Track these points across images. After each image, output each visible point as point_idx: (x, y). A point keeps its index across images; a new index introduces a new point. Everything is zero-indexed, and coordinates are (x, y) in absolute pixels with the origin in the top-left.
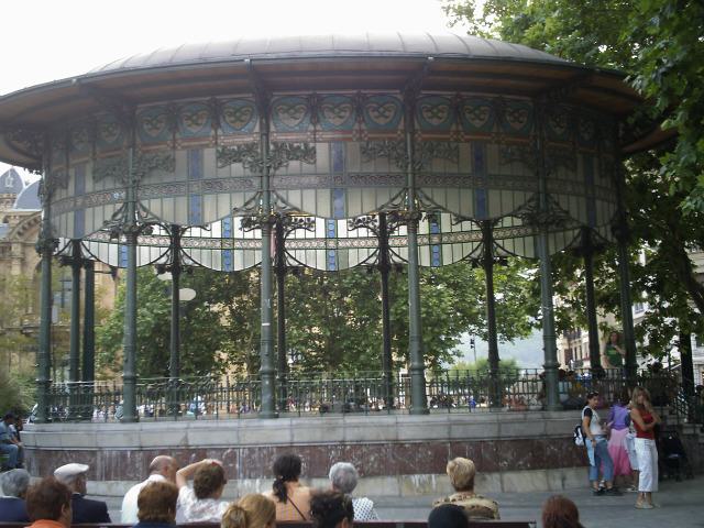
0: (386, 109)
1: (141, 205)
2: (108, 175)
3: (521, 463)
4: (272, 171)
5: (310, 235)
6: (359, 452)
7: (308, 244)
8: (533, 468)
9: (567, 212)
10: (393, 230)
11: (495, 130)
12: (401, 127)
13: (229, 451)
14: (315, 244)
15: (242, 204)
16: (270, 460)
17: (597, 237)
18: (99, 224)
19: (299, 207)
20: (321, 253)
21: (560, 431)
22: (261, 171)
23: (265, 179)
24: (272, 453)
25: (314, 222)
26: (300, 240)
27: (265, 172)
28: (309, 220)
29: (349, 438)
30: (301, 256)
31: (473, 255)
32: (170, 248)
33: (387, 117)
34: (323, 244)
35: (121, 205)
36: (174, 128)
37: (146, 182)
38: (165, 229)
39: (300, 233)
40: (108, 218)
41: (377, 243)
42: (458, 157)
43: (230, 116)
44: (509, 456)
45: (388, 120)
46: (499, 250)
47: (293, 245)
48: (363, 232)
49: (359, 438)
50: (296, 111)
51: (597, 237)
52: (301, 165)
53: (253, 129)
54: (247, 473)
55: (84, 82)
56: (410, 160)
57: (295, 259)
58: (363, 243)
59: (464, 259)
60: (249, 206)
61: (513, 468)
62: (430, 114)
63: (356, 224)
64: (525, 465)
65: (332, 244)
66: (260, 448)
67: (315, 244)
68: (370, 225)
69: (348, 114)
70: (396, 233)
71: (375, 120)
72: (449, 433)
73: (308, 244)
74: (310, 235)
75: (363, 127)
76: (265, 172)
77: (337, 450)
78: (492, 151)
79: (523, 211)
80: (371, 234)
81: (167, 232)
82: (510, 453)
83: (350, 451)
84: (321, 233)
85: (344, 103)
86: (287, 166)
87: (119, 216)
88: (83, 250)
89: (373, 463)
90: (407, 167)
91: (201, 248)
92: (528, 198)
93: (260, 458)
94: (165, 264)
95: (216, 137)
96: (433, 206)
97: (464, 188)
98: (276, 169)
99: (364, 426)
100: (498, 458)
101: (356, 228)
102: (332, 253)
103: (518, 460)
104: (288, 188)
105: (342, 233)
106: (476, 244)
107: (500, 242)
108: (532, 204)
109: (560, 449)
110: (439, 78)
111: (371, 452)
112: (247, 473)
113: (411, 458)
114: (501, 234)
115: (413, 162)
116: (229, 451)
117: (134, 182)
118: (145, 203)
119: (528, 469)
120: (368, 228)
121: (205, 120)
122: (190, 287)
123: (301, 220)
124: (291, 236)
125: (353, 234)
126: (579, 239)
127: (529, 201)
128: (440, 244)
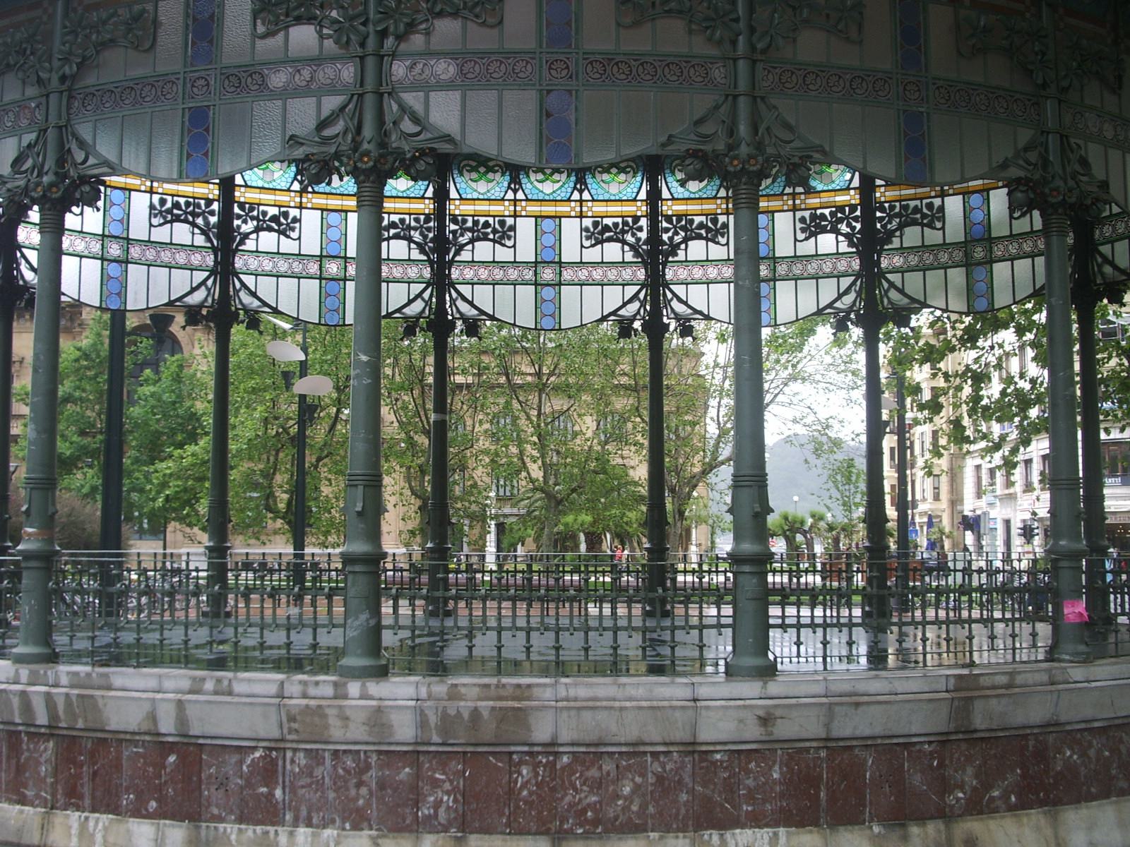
1: (75, 135)
2: (9, 67)
3: (996, 794)
4: (389, 42)
5: (504, 254)
6: (593, 773)
8: (1023, 805)
9: (1104, 185)
10: (674, 249)
13: (257, 754)
14: (513, 274)
15: (312, 124)
16: (360, 784)
17: (1108, 269)
19: (458, 138)
20: (526, 293)
21: (1088, 713)
22: (362, 45)
23: (370, 62)
24: (368, 767)
25: (513, 228)
27: (371, 43)
28: (930, 206)
29: (565, 736)
32: (213, 272)
34: (529, 275)
35: (33, 136)
37: (91, 80)
38: (203, 232)
39: (483, 250)
41: (641, 274)
44: (969, 777)
47: (469, 274)
48: (613, 251)
49: (593, 737)
51: (1108, 269)
52: (464, 29)
54: (304, 812)
56: (742, 25)
58: (612, 274)
60: (327, 132)
61: (978, 807)
65: (548, 274)
66: (336, 753)
67: (513, 274)
68: (629, 238)
72: (827, 726)
74: (504, 254)
76: (371, 43)
77: (536, 765)
79: (1015, 172)
80: (629, 256)
81: (209, 239)
83: (569, 768)
84: (526, 251)
86: (428, 33)
87: (29, 164)
89: (629, 799)
90: (734, 43)
92: (1022, 143)
93: (336, 778)
94: (201, 305)
98: (400, 38)
99: (592, 705)
100: (944, 786)
101: (601, 242)
102: (548, 293)
103: (988, 787)
104: (426, 87)
105: (570, 251)
108: (1033, 156)
109: (1083, 754)
111: (621, 773)
112: (304, 812)
113: (730, 788)
115: (752, 30)
116: (257, 754)
117: (63, 79)
118: (85, 131)
119: (1011, 808)
120: (624, 242)
123: (486, 225)
124: (465, 256)
125: (593, 254)
127: (1026, 149)
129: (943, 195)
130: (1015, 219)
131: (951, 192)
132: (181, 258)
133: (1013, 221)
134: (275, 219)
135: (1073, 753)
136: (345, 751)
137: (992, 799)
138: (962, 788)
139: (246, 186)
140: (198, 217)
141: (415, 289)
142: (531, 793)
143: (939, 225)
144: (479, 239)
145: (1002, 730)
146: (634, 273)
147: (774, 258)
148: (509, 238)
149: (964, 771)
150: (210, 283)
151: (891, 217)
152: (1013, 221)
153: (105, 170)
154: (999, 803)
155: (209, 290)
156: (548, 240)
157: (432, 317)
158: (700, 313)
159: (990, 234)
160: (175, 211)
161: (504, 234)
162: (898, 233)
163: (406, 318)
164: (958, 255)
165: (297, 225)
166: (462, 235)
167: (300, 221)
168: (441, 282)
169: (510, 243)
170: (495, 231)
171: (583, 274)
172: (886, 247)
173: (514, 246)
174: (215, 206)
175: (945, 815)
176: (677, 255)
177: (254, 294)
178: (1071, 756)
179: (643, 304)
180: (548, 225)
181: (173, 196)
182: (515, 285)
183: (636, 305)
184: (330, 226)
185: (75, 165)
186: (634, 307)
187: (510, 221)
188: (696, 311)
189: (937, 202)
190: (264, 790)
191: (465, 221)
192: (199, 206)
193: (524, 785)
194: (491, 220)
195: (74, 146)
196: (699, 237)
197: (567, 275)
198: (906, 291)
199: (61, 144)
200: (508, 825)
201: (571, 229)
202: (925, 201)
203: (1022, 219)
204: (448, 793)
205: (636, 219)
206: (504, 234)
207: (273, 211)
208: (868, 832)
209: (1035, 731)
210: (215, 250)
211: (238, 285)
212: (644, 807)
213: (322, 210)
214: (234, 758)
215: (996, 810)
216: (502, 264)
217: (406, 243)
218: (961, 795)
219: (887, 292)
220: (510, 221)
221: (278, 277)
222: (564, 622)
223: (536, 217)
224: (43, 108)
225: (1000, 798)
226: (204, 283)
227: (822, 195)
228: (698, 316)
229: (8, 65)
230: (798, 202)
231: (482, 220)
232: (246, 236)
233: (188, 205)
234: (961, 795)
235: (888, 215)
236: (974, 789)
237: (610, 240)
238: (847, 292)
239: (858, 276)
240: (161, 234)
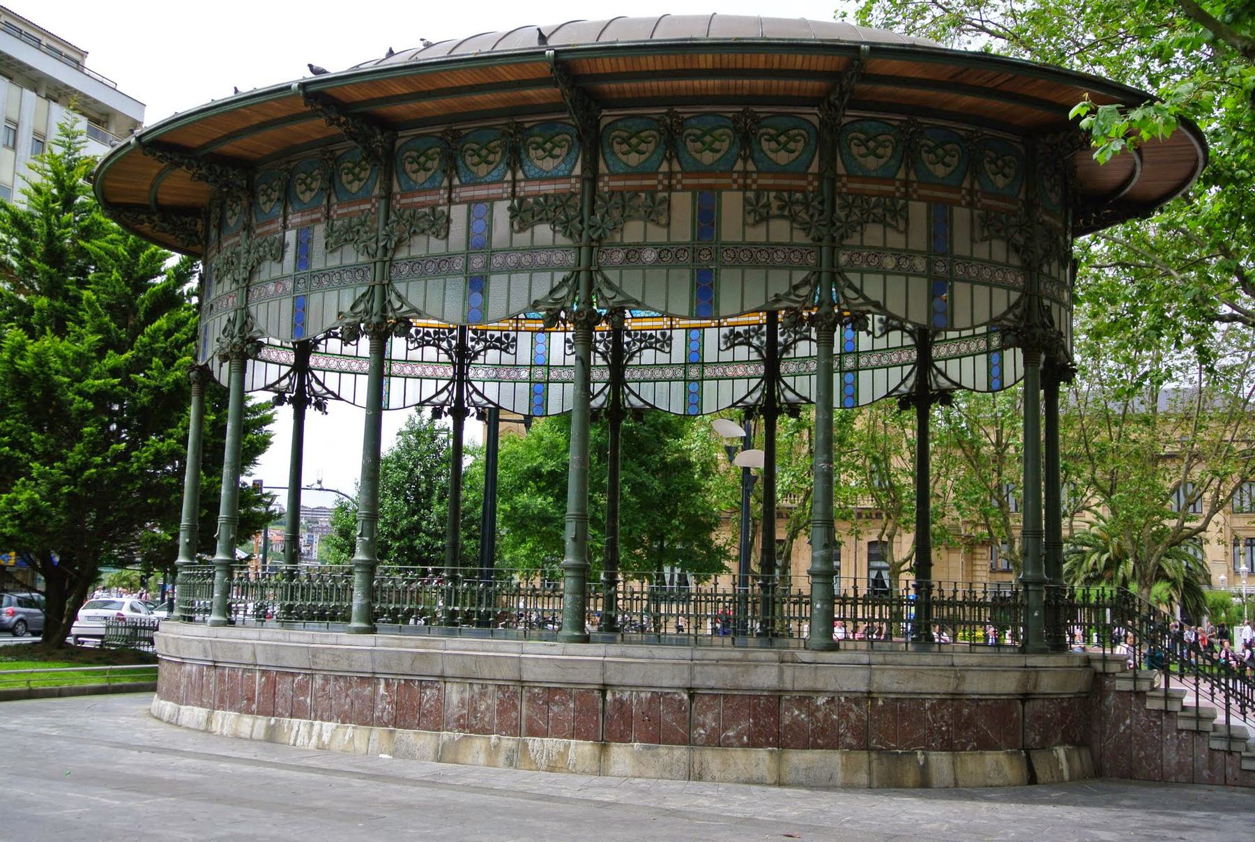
0: (715, 139)
3: (731, 734)
5: (662, 358)
7: (658, 374)
8: (753, 744)
10: (787, 348)
11: (739, 166)
12: (814, 168)
14: (669, 373)
16: (347, 696)
18: (331, 320)
20: (678, 387)
25: (515, 340)
30: (647, 391)
31: (748, 400)
33: (718, 151)
34: (680, 374)
36: (451, 164)
38: (446, 352)
39: (648, 356)
40: (346, 308)
41: (762, 370)
42: (907, 221)
43: (928, 152)
44: (709, 720)
47: (637, 375)
48: (742, 352)
53: (571, 171)
55: (311, 89)
57: (638, 397)
58: (740, 371)
59: (734, 405)
61: (715, 741)
62: (625, 147)
63: (733, 339)
64: (739, 737)
65: (694, 372)
67: (669, 373)
71: (772, 156)
73: (658, 374)
74: (662, 358)
75: (751, 167)
78: (731, 204)
81: (450, 357)
82: (710, 716)
84: (678, 355)
85: (721, 127)
87: (361, 307)
91: (670, 380)
95: (514, 182)
96: (619, 298)
97: (675, 267)
102: (693, 387)
103: (725, 729)
105: (710, 355)
106: (754, 382)
110: (760, 83)
120: (750, 345)
121: (498, 156)
124: (635, 361)
125: (727, 356)
126: (910, 382)
128: (856, 370)
134: (499, 340)
135: (800, 710)
136: (340, 676)
137: (728, 738)
138: (703, 726)
139: (633, 318)
140: (443, 341)
141: (442, 384)
142: (431, 706)
143: (667, 350)
145: (737, 690)
146: (445, 371)
147: (858, 352)
149: (705, 715)
150: (450, 388)
153: (415, 314)
154: (733, 740)
155: (449, 392)
156: (540, 349)
157: (453, 405)
158: (804, 398)
160: (426, 338)
161: (667, 341)
162: (638, 354)
163: (434, 405)
168: (617, 381)
169: (512, 351)
170: (657, 341)
171: (719, 372)
172: (936, 339)
173: (515, 353)
174: (765, 328)
175: (687, 741)
176: (789, 353)
177: (482, 395)
178: (799, 715)
179: (451, 393)
180: (694, 334)
181: (424, 327)
182: (421, 379)
183: (446, 394)
184: (691, 340)
185: (393, 310)
187: (513, 334)
188: (329, 392)
190: (302, 698)
191: (636, 335)
192: (444, 333)
193: (427, 701)
194: (654, 332)
195: (393, 297)
196: (495, 347)
197: (708, 372)
198: (797, 391)
199: (383, 298)
200: (418, 725)
201: (711, 335)
204: (389, 703)
205: (760, 326)
207: (497, 334)
208: (630, 748)
209: (766, 693)
210: (453, 364)
211: (471, 389)
212: (492, 718)
213: (532, 332)
214: (291, 679)
215: (731, 745)
216: (661, 366)
218: (702, 732)
220: (513, 334)
221: (718, 380)
223: (686, 329)
224: (372, 270)
225: (735, 737)
226: (446, 388)
228: (329, 396)
229: (346, 240)
232: (478, 353)
233: (435, 333)
234: (702, 732)
236: (713, 729)
237: (741, 344)
239: (626, 365)
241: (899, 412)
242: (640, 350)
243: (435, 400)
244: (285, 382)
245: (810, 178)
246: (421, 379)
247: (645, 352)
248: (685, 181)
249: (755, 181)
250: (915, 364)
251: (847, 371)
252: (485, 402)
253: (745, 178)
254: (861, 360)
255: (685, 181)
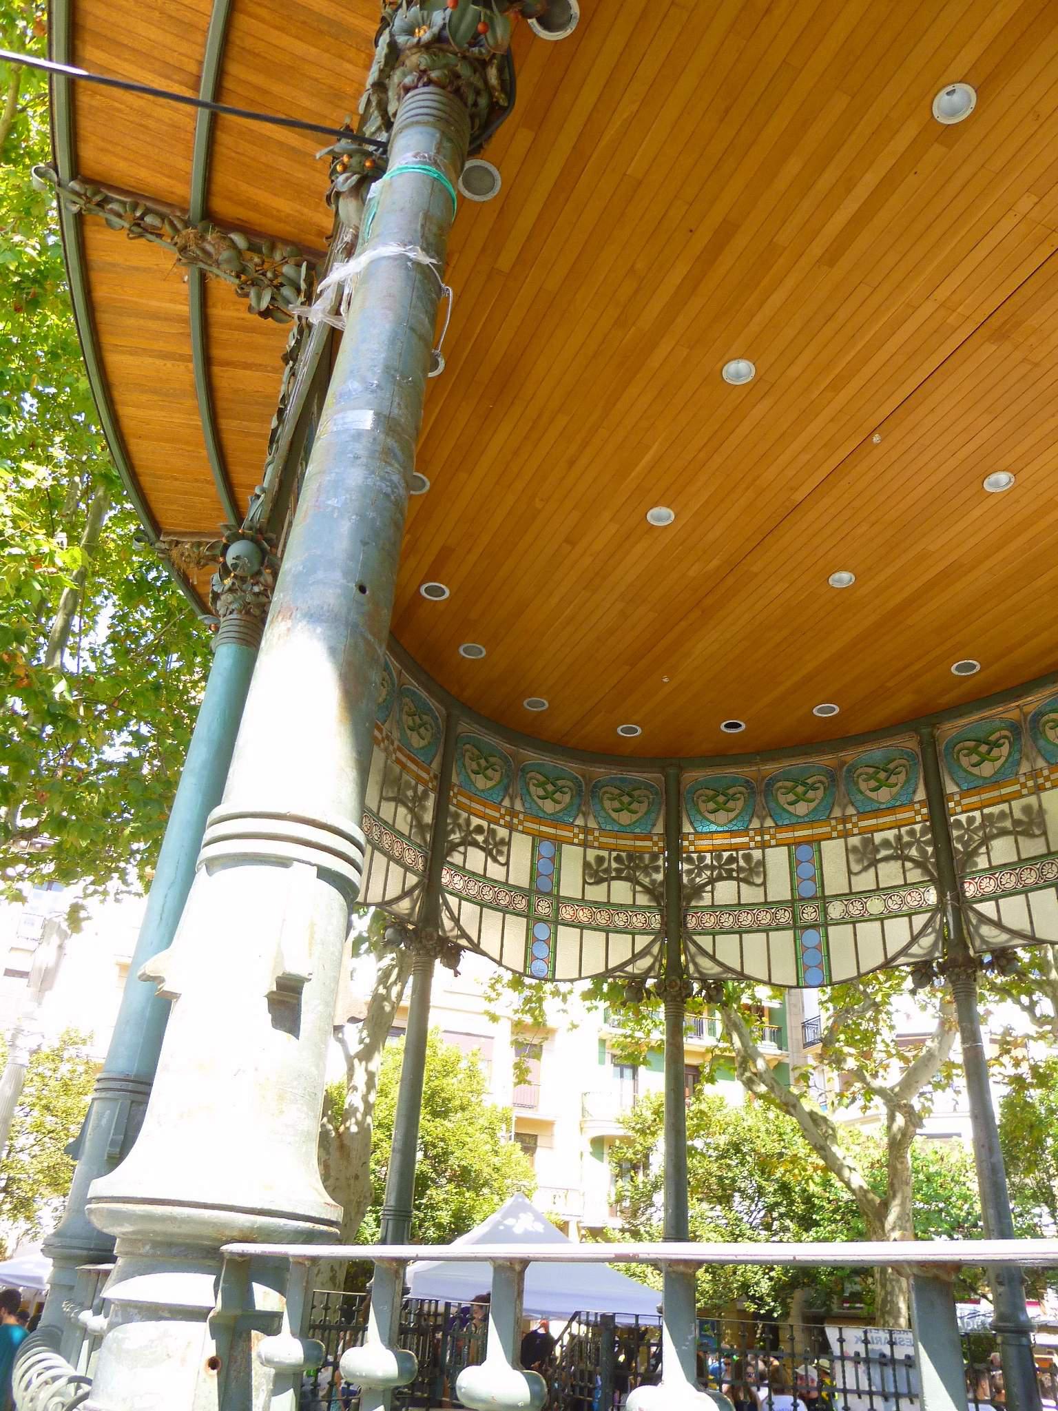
10: (698, 891)
25: (762, 863)
26: (621, 907)
28: (748, 858)
38: (918, 864)
39: (725, 892)
45: (813, 805)
46: (705, 963)
50: (560, 790)
68: (914, 852)
69: (567, 798)
70: (706, 899)
74: (750, 894)
80: (915, 875)
84: (779, 888)
88: (445, 916)
102: (811, 937)
107: (987, 908)
114: (989, 886)
122: (741, 357)
123: (732, 860)
128: (825, 924)
129: (763, 846)
130: (856, 874)
131: (773, 842)
132: (620, 920)
133: (853, 878)
144: (720, 878)
148: (758, 874)
151: (701, 870)
152: (853, 878)
159: (823, 891)
162: (709, 888)
164: (785, 917)
165: (505, 849)
166: (699, 875)
167: (509, 844)
169: (759, 881)
186: (927, 941)
189: (757, 854)
198: (1005, 922)
202: (741, 853)
203: (864, 875)
206: (753, 872)
217: (628, 884)
219: (977, 928)
222: (851, 1384)
227: (715, 836)
230: (581, 836)
231: (726, 855)
235: (698, 867)
238: (922, 933)
240: (596, 893)
241: (186, 242)
242: (712, 881)
243: (629, 969)
244: (405, 905)
245: (655, 838)
246: (851, 893)
247: (719, 885)
248: (602, 840)
249: (752, 839)
250: (658, 934)
251: (807, 927)
252: (717, 969)
253: (763, 841)
254: (831, 909)
255: (602, 840)
